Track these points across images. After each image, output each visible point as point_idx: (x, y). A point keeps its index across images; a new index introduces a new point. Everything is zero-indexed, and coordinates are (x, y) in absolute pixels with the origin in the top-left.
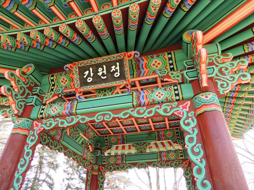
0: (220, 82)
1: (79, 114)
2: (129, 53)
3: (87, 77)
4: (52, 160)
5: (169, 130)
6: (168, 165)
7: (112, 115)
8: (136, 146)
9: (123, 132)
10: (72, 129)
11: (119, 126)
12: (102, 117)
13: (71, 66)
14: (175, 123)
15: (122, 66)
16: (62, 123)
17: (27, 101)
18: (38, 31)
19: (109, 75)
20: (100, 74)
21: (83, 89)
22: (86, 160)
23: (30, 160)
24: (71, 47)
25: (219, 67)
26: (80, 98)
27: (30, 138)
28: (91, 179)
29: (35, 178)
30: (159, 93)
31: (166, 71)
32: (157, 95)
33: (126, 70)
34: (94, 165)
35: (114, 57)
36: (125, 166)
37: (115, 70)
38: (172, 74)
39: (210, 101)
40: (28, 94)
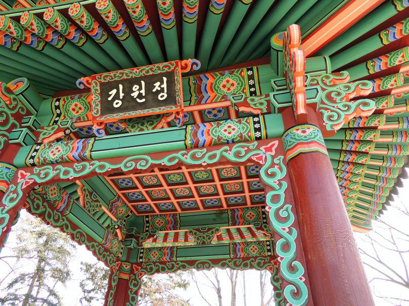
0: (328, 112)
1: (95, 160)
2: (184, 62)
3: (114, 99)
4: (59, 266)
5: (250, 209)
6: (246, 265)
7: (151, 161)
8: (195, 233)
9: (176, 210)
10: (89, 197)
11: (169, 199)
12: (134, 164)
13: (87, 81)
14: (261, 197)
15: (171, 84)
16: (66, 173)
17: (11, 136)
18: (35, 14)
19: (150, 97)
20: (135, 95)
21: (106, 117)
22: (111, 253)
23: (4, 231)
24: (89, 48)
25: (326, 92)
26: (99, 133)
27: (8, 196)
28: (117, 286)
29: (28, 296)
30: (229, 127)
31: (242, 96)
32: (225, 130)
33: (177, 89)
34: (123, 263)
35: (160, 67)
36: (176, 266)
37: (159, 89)
38: (253, 100)
39: (310, 138)
40: (14, 126)
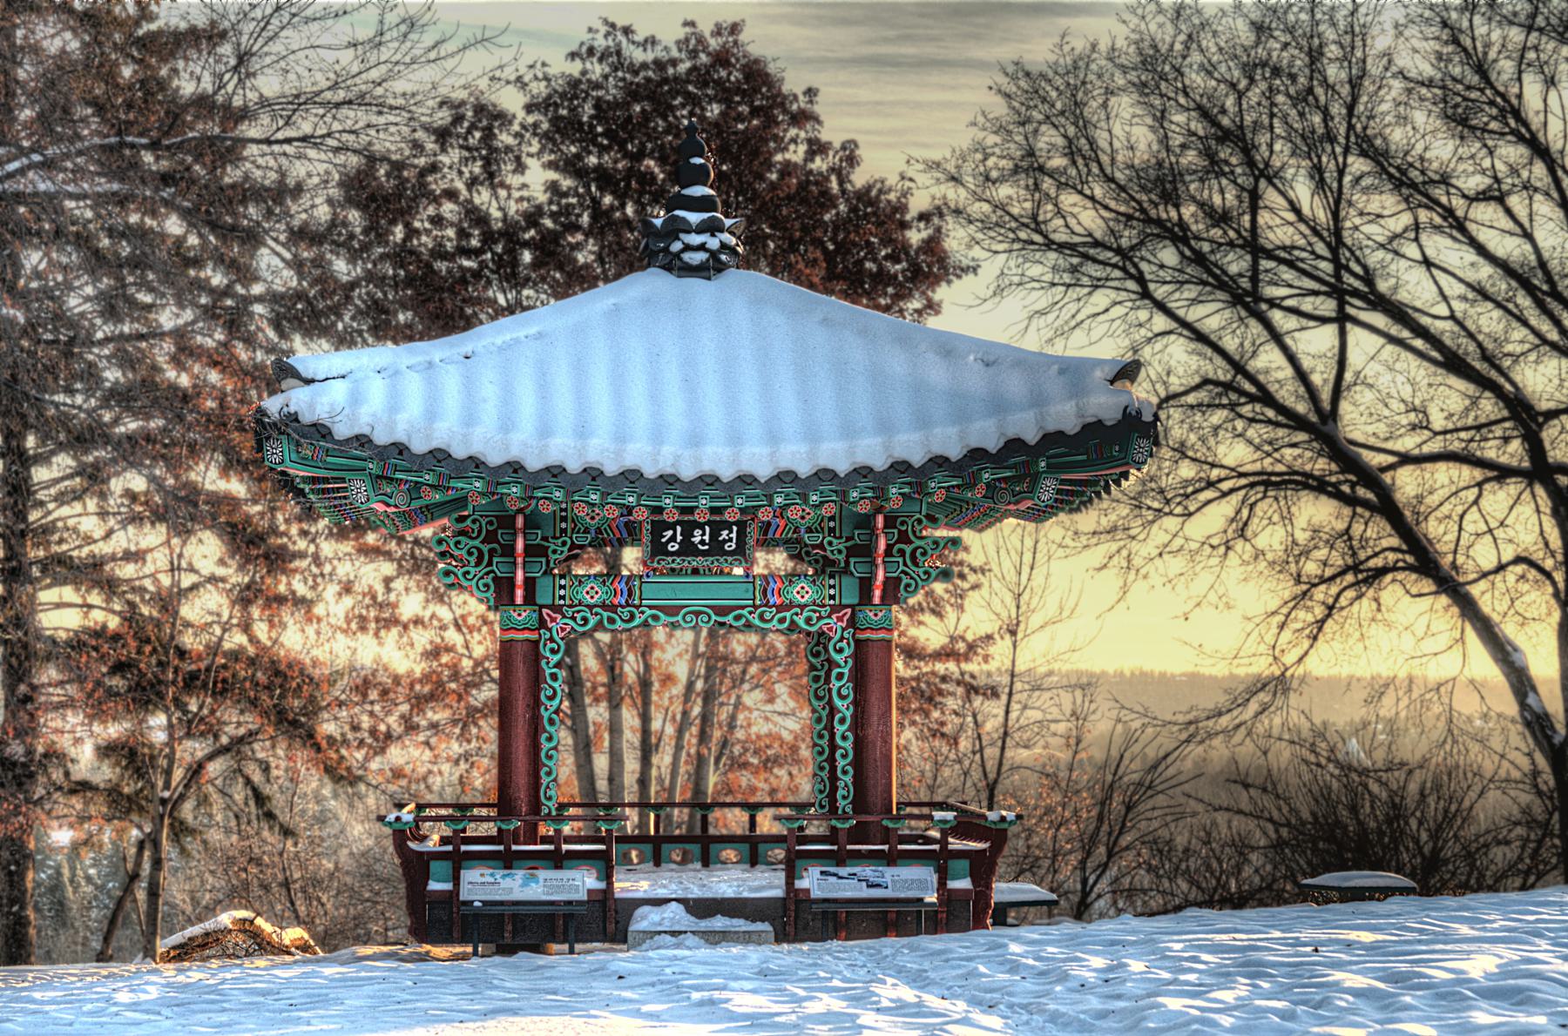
7: (714, 617)
20: (697, 540)
